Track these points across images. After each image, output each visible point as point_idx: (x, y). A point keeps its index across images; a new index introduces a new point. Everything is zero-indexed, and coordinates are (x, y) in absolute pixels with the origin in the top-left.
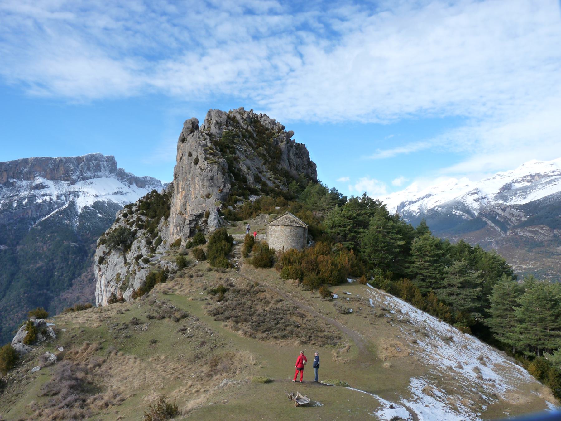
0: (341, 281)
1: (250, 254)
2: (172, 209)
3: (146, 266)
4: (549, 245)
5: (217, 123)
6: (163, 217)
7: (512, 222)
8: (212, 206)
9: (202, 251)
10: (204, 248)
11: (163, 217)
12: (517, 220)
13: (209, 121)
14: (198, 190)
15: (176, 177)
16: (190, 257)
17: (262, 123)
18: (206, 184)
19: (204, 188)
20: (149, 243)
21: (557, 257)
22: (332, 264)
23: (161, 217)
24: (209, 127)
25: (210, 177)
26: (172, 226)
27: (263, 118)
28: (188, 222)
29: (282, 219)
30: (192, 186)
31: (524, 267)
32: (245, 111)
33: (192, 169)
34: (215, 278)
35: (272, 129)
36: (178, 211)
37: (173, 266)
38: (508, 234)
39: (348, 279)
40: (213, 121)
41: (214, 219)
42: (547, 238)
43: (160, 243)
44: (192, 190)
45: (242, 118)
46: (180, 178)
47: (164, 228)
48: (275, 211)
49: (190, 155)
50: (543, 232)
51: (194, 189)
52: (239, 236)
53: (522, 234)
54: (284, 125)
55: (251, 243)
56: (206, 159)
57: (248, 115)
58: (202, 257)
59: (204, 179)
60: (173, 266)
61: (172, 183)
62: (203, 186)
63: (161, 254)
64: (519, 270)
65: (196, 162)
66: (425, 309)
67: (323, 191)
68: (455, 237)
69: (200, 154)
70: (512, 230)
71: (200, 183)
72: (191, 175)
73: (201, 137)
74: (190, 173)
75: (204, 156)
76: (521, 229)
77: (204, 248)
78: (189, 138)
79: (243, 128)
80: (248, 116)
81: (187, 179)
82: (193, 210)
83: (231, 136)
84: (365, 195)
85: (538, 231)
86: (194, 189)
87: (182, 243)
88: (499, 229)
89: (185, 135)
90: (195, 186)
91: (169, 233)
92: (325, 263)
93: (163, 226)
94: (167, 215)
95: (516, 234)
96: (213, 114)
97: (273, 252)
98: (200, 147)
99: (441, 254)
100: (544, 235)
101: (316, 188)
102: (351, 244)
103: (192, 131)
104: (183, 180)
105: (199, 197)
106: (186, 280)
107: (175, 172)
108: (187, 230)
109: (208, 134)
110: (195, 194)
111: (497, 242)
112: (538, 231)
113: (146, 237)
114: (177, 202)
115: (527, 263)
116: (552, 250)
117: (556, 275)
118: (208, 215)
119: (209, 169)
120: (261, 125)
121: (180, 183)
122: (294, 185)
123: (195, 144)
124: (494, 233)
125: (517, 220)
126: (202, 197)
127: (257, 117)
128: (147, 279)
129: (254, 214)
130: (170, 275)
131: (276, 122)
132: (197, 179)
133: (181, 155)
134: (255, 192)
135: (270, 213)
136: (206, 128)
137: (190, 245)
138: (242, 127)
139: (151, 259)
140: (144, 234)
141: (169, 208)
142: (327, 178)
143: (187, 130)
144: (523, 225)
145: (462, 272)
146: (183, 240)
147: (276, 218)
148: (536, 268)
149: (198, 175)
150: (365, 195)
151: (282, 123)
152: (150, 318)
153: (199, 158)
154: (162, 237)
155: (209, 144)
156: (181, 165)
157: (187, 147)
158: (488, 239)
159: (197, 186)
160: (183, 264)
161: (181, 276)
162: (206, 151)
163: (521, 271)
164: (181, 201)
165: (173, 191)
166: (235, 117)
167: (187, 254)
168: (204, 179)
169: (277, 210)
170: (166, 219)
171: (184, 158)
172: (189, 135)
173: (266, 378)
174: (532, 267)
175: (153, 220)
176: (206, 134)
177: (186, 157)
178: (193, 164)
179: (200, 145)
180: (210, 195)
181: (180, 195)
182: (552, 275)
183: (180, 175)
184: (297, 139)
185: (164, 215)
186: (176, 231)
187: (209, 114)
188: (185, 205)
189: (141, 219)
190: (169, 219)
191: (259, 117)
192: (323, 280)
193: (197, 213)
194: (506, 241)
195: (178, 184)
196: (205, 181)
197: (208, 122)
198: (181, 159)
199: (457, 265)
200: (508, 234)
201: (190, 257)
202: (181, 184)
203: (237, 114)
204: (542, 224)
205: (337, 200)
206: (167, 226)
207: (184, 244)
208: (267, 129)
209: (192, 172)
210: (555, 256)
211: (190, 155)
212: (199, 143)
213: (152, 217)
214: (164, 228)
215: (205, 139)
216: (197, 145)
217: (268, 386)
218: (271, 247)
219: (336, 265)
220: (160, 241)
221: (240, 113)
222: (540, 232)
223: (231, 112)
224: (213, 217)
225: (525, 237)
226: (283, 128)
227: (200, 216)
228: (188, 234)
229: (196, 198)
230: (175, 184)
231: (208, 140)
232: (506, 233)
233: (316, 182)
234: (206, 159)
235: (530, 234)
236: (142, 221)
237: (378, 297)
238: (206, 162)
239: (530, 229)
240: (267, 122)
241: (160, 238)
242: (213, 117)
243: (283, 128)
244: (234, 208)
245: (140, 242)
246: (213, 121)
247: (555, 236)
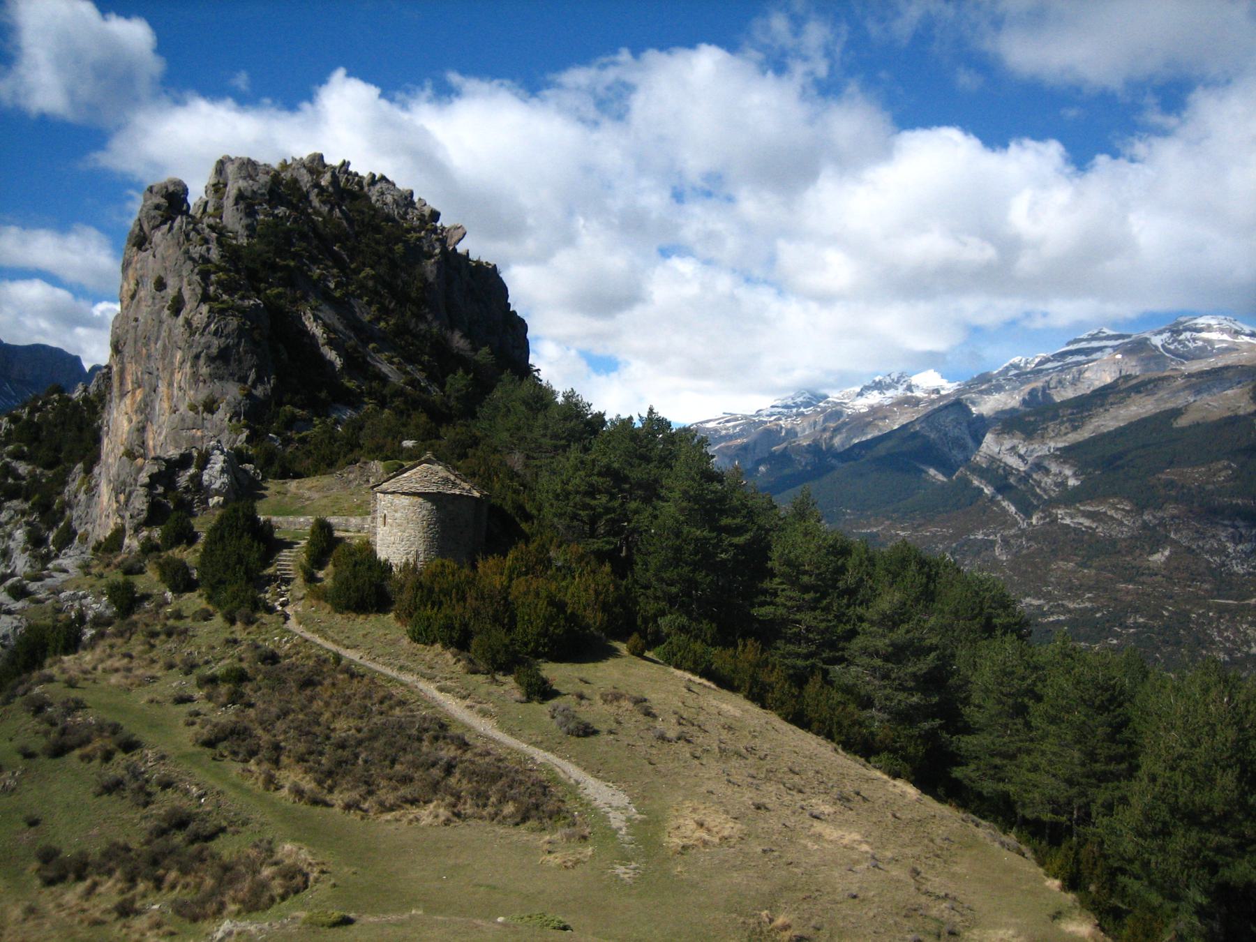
0: (582, 646)
1: (321, 574)
2: (106, 441)
3: (19, 605)
4: (1130, 551)
5: (240, 197)
6: (80, 466)
7: (1045, 490)
8: (221, 435)
9: (182, 568)
10: (189, 556)
11: (80, 466)
12: (1057, 484)
13: (218, 188)
14: (180, 388)
15: (117, 348)
16: (149, 580)
17: (374, 199)
18: (204, 370)
19: (196, 382)
20: (35, 541)
21: (1149, 580)
22: (552, 602)
23: (75, 464)
24: (219, 208)
25: (214, 351)
26: (105, 491)
27: (378, 186)
28: (144, 478)
29: (414, 477)
30: (165, 375)
31: (1071, 606)
32: (325, 166)
33: (165, 326)
34: (212, 637)
35: (404, 217)
36: (122, 449)
37: (97, 606)
38: (1034, 521)
39: (93, 632)
40: (232, 190)
41: (223, 471)
42: (1126, 532)
43: (71, 540)
44: (162, 388)
45: (317, 185)
46: (128, 351)
47: (82, 497)
48: (402, 450)
49: (160, 285)
50: (1118, 516)
51: (170, 385)
52: (295, 526)
53: (1068, 521)
54: (438, 209)
55: (325, 542)
56: (205, 298)
57: (334, 175)
58: (181, 581)
59: (197, 357)
60: (97, 606)
61: (109, 367)
62: (195, 378)
63: (65, 571)
64: (1058, 613)
65: (177, 307)
66: (799, 720)
67: (541, 397)
68: (903, 529)
69: (185, 283)
70: (1043, 511)
71: (187, 368)
72: (160, 344)
73: (192, 234)
74: (157, 339)
75: (199, 291)
76: (1067, 506)
77: (189, 556)
78: (158, 236)
79: (318, 213)
80: (335, 180)
81: (149, 356)
82: (163, 442)
83: (278, 237)
84: (651, 411)
85: (1105, 513)
86: (170, 385)
87: (127, 541)
88: (1013, 509)
89: (146, 227)
90: (172, 374)
91: (95, 512)
92: (531, 598)
93: (78, 491)
94: (92, 458)
95: (1054, 521)
96: (230, 169)
97: (386, 568)
98: (189, 264)
99: (837, 578)
100: (1121, 523)
101: (525, 389)
102: (608, 543)
103: (168, 218)
104: (136, 358)
105: (183, 408)
106: (137, 645)
107: (114, 334)
108: (140, 503)
109: (212, 228)
110: (170, 398)
111: (1006, 541)
112: (1105, 513)
113: (27, 523)
114: (119, 421)
115: (1078, 596)
116: (1137, 563)
117: (1145, 625)
118: (204, 460)
119: (213, 327)
120: (372, 207)
121: (128, 366)
122: (458, 381)
123: (174, 254)
124: (1004, 520)
125: (1057, 484)
126: (193, 408)
127: (360, 183)
128: (19, 643)
129: (341, 462)
130: (89, 632)
131: (416, 199)
132: (179, 355)
133: (132, 286)
134: (353, 400)
135: (385, 459)
136: (210, 209)
137: (149, 548)
138: (314, 208)
139: (33, 586)
140: (23, 513)
141: (98, 440)
142: (553, 363)
143: (153, 213)
144: (1070, 498)
145: (892, 621)
146: (129, 532)
147: (401, 470)
148: (1098, 610)
149: (181, 344)
150: (651, 411)
151: (433, 204)
152: (28, 755)
153: (187, 294)
154: (75, 524)
155: (215, 254)
156: (132, 314)
157: (150, 264)
158: (986, 535)
159: (178, 376)
160: (127, 600)
161: (120, 634)
162: (205, 275)
163: (1062, 618)
164: (130, 421)
165: (109, 387)
166: (295, 181)
167: (141, 571)
168: (197, 357)
169: (409, 449)
170: (88, 471)
171: (142, 293)
172: (157, 227)
173: (336, 914)
174: (1088, 605)
175: (50, 473)
176: (210, 226)
177: (147, 290)
178: (166, 312)
179: (191, 259)
180: (214, 401)
181: (128, 400)
182: (1137, 625)
183: (130, 343)
184: (474, 247)
185: (81, 458)
186: (115, 506)
187: (221, 166)
188: (142, 430)
189: (15, 470)
190: (96, 470)
191: (365, 183)
192: (524, 647)
193: (173, 453)
194: (1028, 540)
195: (122, 372)
196: (202, 361)
197: (216, 191)
198: (133, 297)
199: (888, 601)
200: (1034, 521)
201: (149, 580)
202: (132, 369)
203: (303, 171)
204: (1115, 495)
205: (581, 425)
206: (91, 491)
207: (132, 543)
208: (389, 218)
209: (164, 334)
210: (1144, 578)
211: (160, 285)
212: (187, 252)
213: (49, 466)
214: (82, 497)
215: (206, 241)
216: (182, 259)
217: (340, 931)
218: (382, 554)
219: (561, 606)
220: (67, 537)
221: (311, 171)
222: (1112, 518)
223: (285, 166)
224: (218, 467)
225: (1075, 529)
226: (435, 215)
227: (184, 461)
228: (144, 515)
229: (163, 414)
230: (115, 369)
231: (213, 246)
232: (1031, 518)
233: (525, 371)
234: (205, 298)
235: (1087, 522)
236: (18, 477)
237: (667, 686)
238: (205, 309)
239: (1090, 509)
240: (389, 199)
241: (69, 525)
242: (231, 177)
243: (435, 215)
244: (287, 442)
245: (10, 536)
246: (232, 190)
247: (1145, 526)
